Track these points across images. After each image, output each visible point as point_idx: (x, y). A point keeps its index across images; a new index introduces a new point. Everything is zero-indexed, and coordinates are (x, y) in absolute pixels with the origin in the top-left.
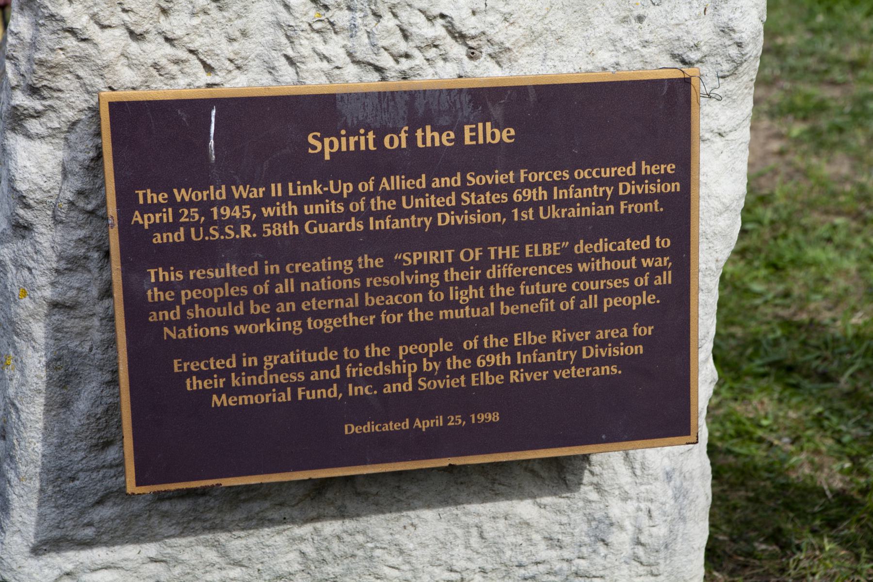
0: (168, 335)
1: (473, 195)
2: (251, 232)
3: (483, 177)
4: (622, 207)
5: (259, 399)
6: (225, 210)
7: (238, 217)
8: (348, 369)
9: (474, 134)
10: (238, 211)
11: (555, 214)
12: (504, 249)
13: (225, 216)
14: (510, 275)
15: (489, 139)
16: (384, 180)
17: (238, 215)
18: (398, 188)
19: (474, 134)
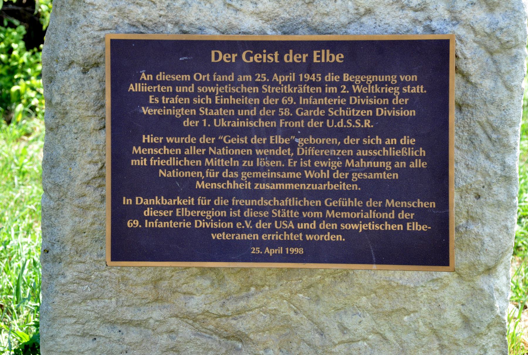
0: (161, 174)
1: (207, 110)
2: (370, 124)
3: (206, 88)
4: (281, 123)
5: (353, 216)
6: (307, 76)
7: (314, 80)
8: (151, 160)
9: (319, 56)
10: (314, 77)
11: (224, 124)
12: (146, 137)
13: (306, 79)
14: (313, 154)
15: (328, 60)
16: (132, 85)
17: (314, 79)
18: (139, 90)
19: (319, 56)
